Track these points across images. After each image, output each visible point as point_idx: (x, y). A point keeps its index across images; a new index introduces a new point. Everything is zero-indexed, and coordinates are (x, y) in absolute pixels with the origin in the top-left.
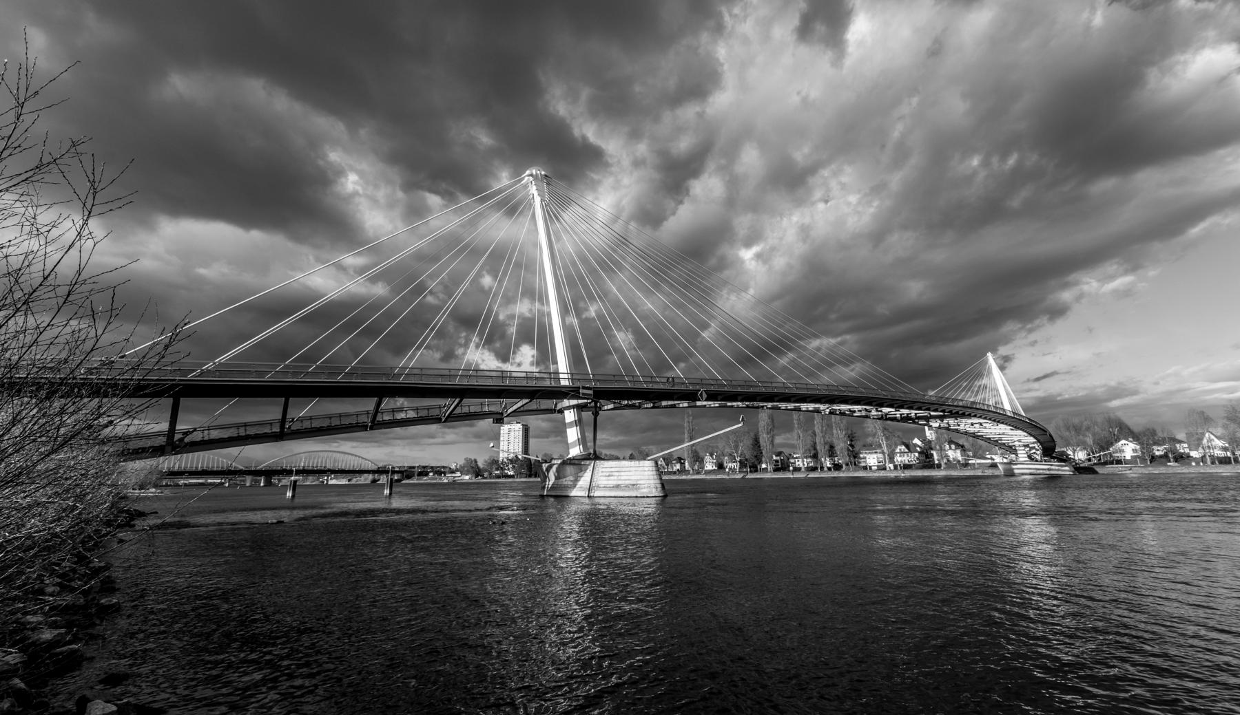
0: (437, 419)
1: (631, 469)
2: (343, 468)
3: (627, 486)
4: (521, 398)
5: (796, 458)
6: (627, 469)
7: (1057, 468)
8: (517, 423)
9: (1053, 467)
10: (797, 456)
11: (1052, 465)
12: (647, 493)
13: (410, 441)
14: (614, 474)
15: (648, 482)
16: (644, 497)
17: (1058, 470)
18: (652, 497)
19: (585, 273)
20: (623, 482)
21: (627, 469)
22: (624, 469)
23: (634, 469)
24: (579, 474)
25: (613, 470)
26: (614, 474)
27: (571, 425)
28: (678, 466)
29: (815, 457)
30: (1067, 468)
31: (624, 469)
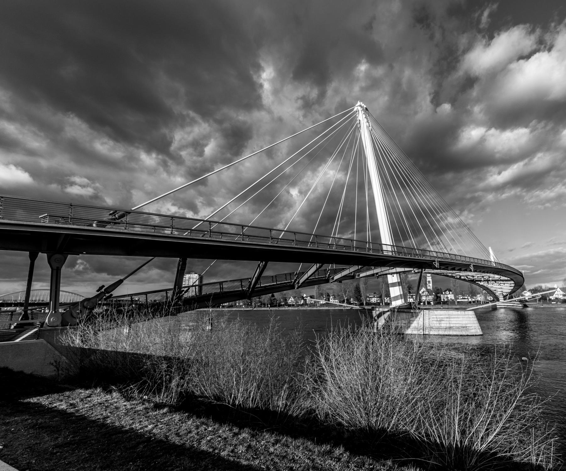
0: (325, 280)
1: (459, 316)
2: (65, 302)
3: (458, 328)
4: (354, 264)
5: (371, 297)
6: (456, 316)
7: (516, 305)
8: (195, 273)
9: (515, 305)
10: (371, 296)
11: (514, 303)
12: (476, 333)
13: (89, 283)
14: (444, 319)
15: (474, 325)
16: (473, 335)
17: (517, 306)
18: (479, 335)
19: (332, 158)
20: (454, 325)
21: (456, 316)
22: (452, 317)
23: (461, 316)
24: (411, 319)
25: (442, 316)
26: (444, 319)
27: (394, 285)
28: (302, 302)
29: (381, 297)
30: (521, 305)
31: (452, 317)
